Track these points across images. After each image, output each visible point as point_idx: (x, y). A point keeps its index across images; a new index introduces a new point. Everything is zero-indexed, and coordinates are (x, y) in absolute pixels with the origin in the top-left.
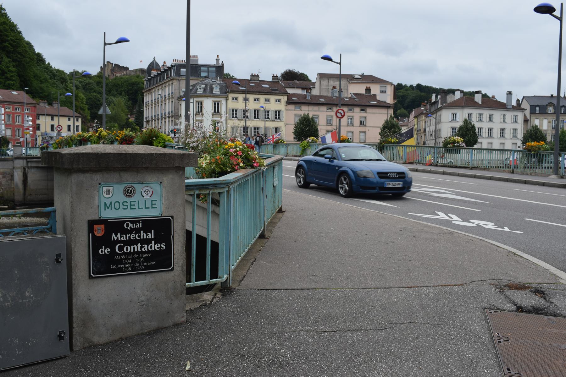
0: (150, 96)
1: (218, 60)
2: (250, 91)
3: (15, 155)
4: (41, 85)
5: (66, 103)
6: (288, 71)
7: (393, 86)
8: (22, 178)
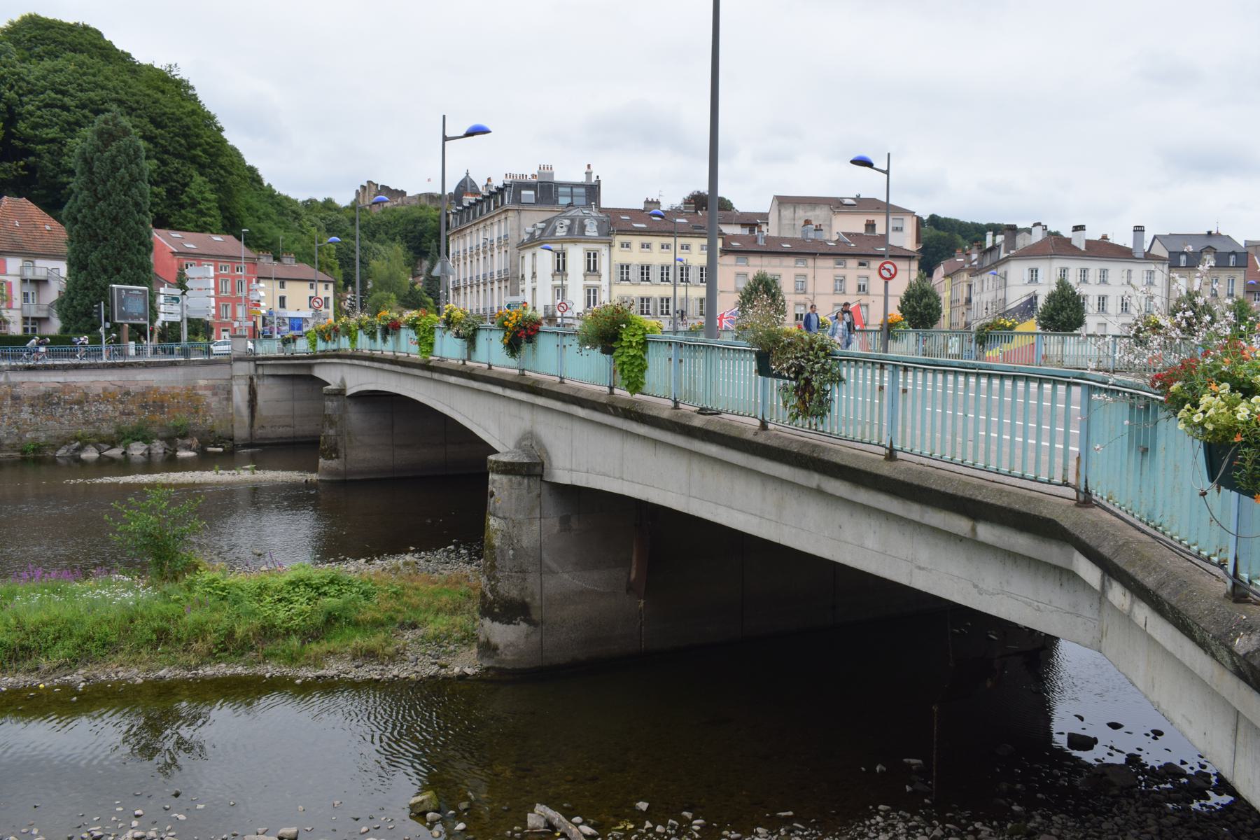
0: (461, 241)
1: (589, 174)
2: (653, 230)
3: (235, 353)
4: (259, 225)
5: (304, 257)
6: (696, 193)
7: (915, 218)
8: (247, 397)
